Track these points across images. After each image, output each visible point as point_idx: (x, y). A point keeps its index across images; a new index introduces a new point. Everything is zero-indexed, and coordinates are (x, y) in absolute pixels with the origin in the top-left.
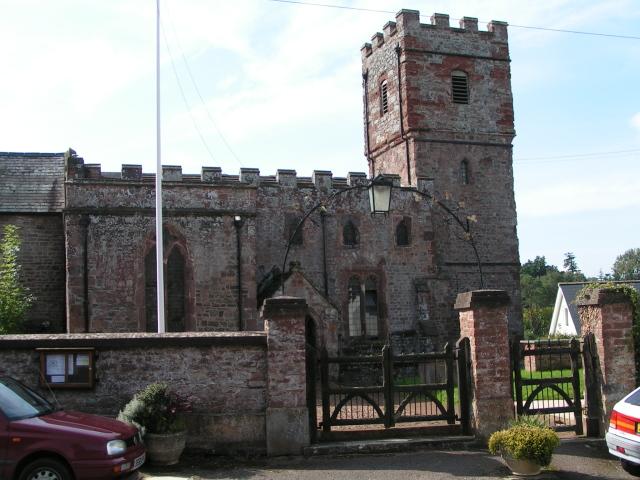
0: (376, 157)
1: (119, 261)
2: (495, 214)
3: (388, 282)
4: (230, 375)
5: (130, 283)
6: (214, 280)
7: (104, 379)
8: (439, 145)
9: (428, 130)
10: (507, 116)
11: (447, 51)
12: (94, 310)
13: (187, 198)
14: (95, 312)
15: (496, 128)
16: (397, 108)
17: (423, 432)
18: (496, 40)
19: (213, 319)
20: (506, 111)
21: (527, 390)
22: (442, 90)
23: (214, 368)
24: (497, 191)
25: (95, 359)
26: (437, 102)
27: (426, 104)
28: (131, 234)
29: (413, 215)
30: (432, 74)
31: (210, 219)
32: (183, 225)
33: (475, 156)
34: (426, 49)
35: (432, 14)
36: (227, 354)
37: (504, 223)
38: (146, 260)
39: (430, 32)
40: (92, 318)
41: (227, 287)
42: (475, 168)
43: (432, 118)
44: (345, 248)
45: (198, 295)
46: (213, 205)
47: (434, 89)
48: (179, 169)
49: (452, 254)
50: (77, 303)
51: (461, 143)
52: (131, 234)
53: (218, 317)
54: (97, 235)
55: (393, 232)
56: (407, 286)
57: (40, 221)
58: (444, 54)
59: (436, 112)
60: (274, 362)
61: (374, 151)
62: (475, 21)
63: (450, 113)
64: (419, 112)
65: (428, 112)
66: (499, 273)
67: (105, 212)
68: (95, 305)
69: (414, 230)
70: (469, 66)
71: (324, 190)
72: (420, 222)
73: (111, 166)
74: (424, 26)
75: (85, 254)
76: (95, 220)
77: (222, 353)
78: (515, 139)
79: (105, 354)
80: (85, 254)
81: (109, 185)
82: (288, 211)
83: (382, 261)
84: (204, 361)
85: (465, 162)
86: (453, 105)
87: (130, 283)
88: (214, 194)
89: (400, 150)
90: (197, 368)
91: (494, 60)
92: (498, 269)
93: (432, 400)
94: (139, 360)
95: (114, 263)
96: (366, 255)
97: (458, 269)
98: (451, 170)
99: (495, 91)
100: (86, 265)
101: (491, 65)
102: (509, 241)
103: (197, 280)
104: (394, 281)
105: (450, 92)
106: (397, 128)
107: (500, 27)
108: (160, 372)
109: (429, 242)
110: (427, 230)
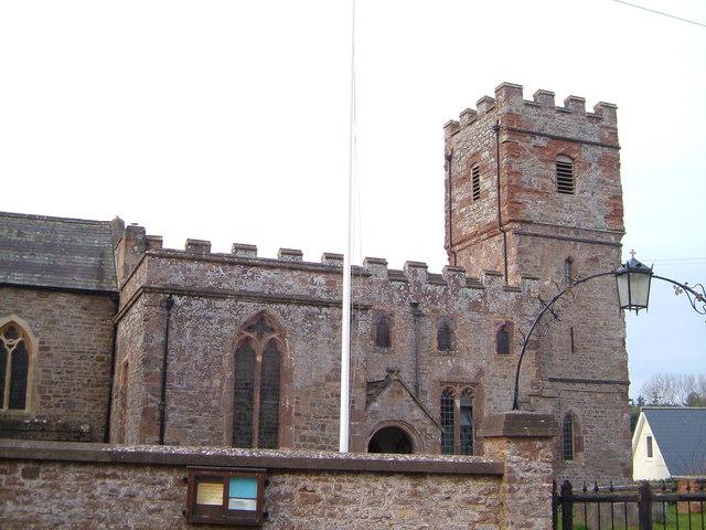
1: (206, 354)
2: (601, 324)
4: (450, 515)
5: (217, 382)
6: (317, 384)
7: (275, 512)
9: (530, 223)
11: (552, 133)
13: (290, 282)
14: (173, 418)
16: (493, 194)
19: (313, 433)
22: (547, 177)
23: (428, 504)
24: (604, 296)
25: (263, 485)
27: (528, 191)
28: (221, 322)
29: (516, 319)
31: (316, 309)
32: (283, 313)
33: (581, 255)
35: (535, 90)
36: (447, 486)
37: (611, 333)
38: (235, 356)
39: (533, 111)
40: (168, 424)
43: (534, 209)
44: (440, 355)
45: (297, 403)
46: (319, 293)
47: (537, 175)
48: (207, 245)
49: (553, 368)
50: (153, 405)
52: (221, 322)
53: (319, 430)
54: (181, 320)
57: (86, 301)
60: (513, 498)
61: (459, 243)
63: (555, 204)
67: (192, 293)
68: (172, 409)
69: (517, 338)
71: (418, 285)
72: (522, 328)
73: (175, 242)
74: (528, 104)
75: (166, 343)
76: (178, 301)
79: (279, 478)
80: (166, 343)
81: (199, 260)
83: (481, 373)
84: (415, 494)
85: (569, 261)
86: (557, 195)
88: (320, 279)
89: (495, 245)
90: (406, 503)
91: (603, 146)
92: (605, 387)
95: (199, 357)
96: (463, 364)
100: (166, 359)
101: (599, 151)
102: (617, 355)
103: (297, 384)
104: (492, 396)
105: (555, 179)
106: (493, 217)
107: (607, 112)
108: (354, 507)
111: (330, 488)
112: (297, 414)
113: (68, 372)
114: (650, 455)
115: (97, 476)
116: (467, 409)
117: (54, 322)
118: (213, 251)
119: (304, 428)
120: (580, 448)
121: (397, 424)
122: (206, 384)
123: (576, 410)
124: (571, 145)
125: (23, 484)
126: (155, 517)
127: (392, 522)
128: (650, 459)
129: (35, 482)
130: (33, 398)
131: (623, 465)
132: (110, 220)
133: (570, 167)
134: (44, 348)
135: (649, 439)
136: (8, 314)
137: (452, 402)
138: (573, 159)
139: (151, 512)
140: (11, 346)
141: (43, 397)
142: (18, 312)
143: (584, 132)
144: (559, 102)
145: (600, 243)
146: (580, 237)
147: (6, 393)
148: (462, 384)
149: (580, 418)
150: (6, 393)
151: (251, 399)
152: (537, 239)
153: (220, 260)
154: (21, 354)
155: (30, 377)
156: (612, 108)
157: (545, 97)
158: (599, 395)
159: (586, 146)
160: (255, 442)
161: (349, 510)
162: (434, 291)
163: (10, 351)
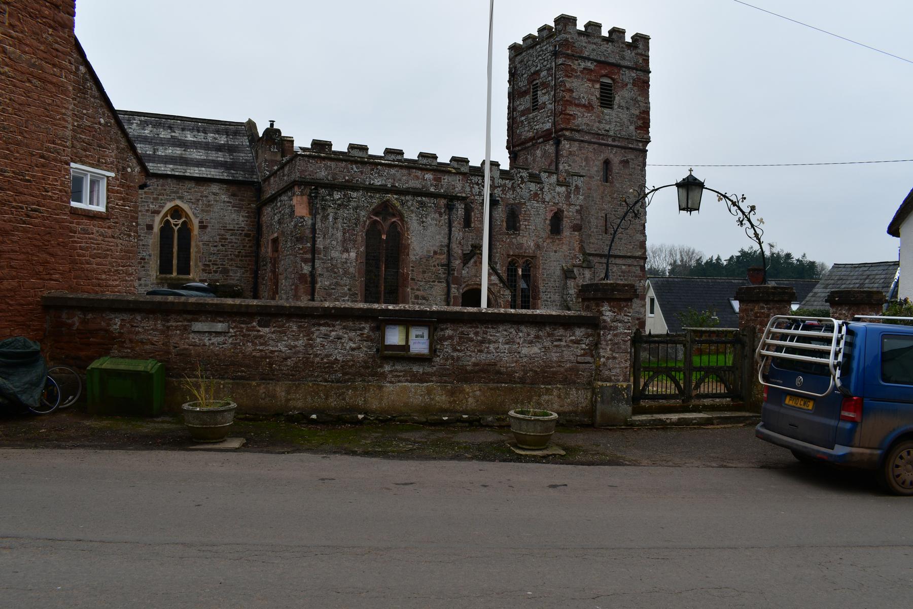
0: (519, 151)
8: (586, 145)
9: (578, 131)
12: (319, 279)
15: (634, 133)
17: (712, 408)
18: (640, 51)
21: (695, 376)
27: (578, 105)
32: (403, 204)
33: (616, 159)
41: (438, 265)
42: (616, 167)
44: (508, 234)
45: (413, 271)
48: (330, 145)
55: (548, 222)
56: (558, 272)
58: (595, 61)
59: (586, 114)
61: (518, 145)
65: (579, 114)
66: (629, 266)
67: (332, 187)
68: (321, 275)
69: (566, 223)
74: (580, 33)
75: (314, 225)
77: (555, 330)
80: (314, 225)
83: (538, 246)
84: (537, 337)
85: (607, 163)
87: (353, 255)
88: (429, 176)
90: (531, 342)
91: (637, 70)
92: (629, 261)
93: (723, 383)
94: (476, 334)
96: (524, 241)
98: (595, 169)
103: (412, 258)
105: (598, 96)
107: (641, 41)
111: (246, 330)
112: (413, 279)
113: (222, 245)
115: (314, 325)
116: (526, 276)
117: (209, 206)
118: (333, 149)
119: (418, 290)
122: (345, 255)
125: (259, 331)
126: (355, 353)
127: (522, 355)
129: (267, 330)
130: (196, 265)
131: (638, 319)
132: (245, 122)
133: (611, 87)
134: (203, 227)
135: (652, 300)
136: (174, 199)
137: (516, 271)
138: (613, 79)
139: (353, 349)
140: (176, 225)
141: (205, 265)
142: (181, 198)
146: (616, 143)
147: (175, 262)
148: (523, 257)
150: (175, 262)
151: (378, 267)
153: (339, 157)
154: (185, 230)
155: (193, 250)
157: (594, 27)
158: (624, 267)
159: (624, 69)
160: (382, 300)
161: (492, 347)
163: (176, 229)
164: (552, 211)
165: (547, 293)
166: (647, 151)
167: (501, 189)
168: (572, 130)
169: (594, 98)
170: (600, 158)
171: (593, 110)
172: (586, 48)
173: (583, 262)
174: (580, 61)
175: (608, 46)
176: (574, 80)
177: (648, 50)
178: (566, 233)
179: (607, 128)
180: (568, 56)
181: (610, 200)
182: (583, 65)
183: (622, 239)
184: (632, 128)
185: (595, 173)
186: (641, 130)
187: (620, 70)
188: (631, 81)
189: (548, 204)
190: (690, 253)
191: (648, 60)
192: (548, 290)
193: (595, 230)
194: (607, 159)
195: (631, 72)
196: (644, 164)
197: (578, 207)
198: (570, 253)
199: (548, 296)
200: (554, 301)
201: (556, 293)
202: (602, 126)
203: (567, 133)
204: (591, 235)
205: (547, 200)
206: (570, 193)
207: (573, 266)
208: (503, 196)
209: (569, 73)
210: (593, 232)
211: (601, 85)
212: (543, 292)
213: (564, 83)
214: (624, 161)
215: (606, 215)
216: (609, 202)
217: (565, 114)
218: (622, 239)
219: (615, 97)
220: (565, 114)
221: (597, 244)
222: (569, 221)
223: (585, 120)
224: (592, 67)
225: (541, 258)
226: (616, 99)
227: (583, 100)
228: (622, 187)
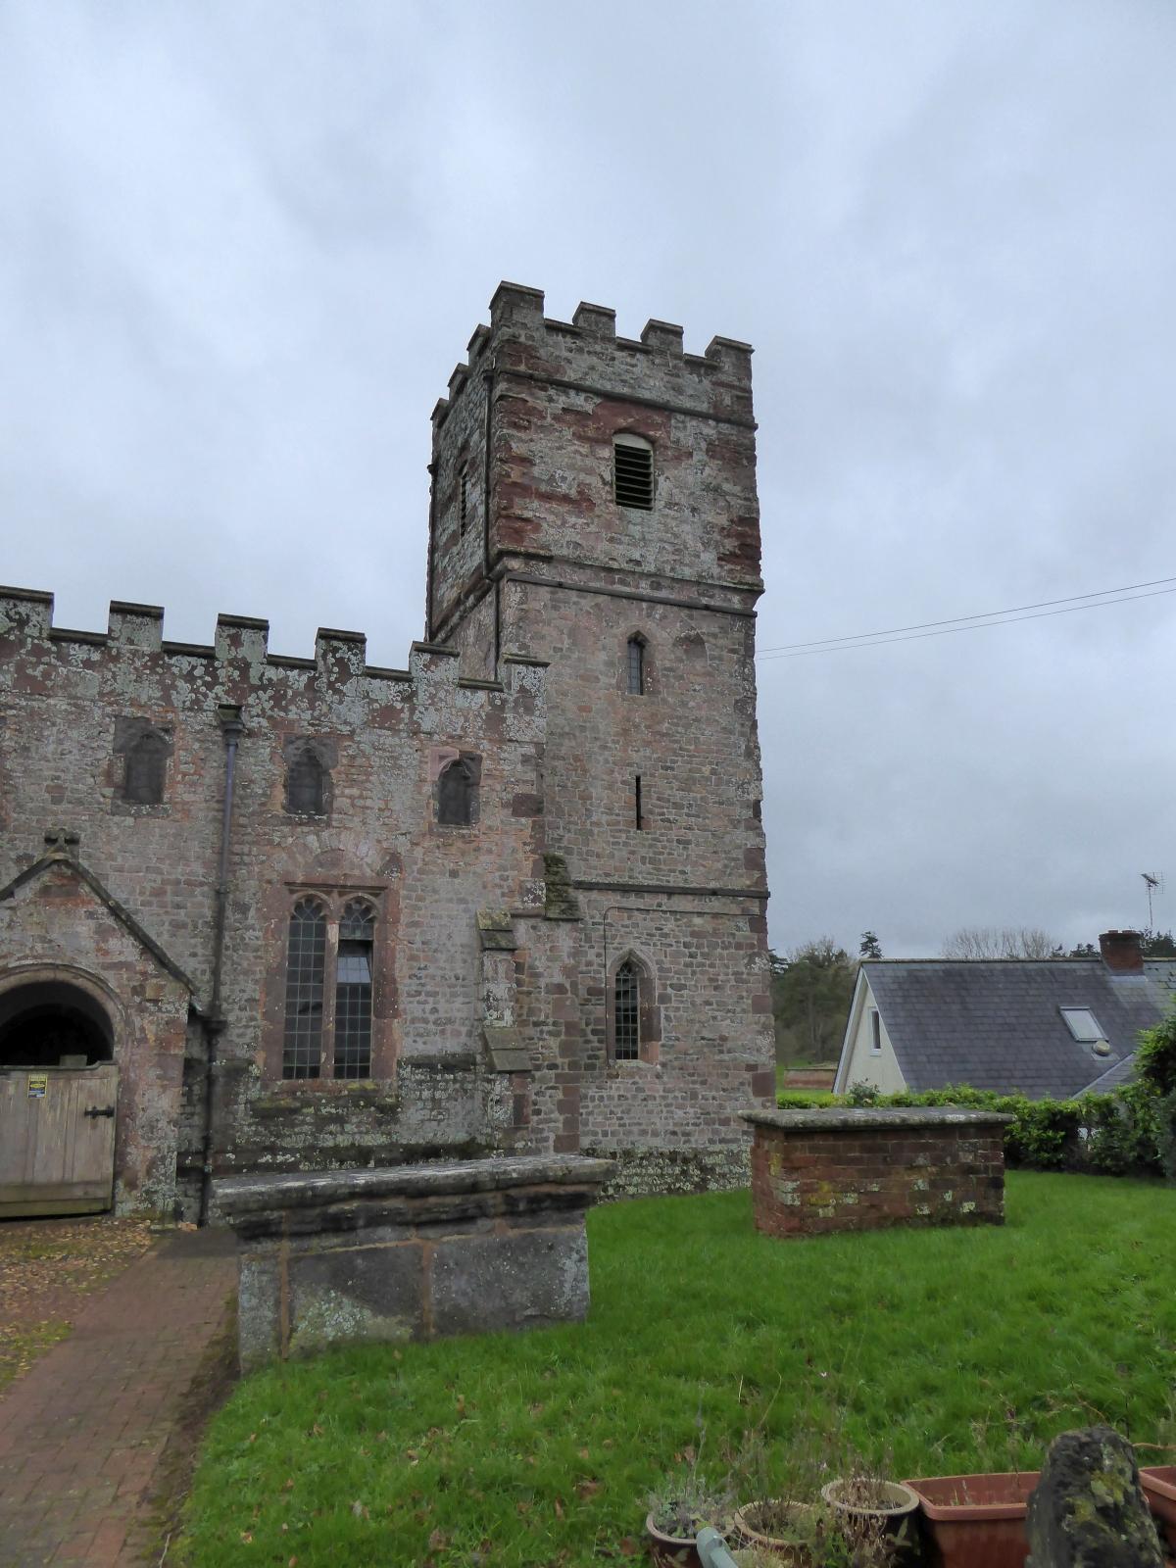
2: (706, 770)
3: (404, 919)
8: (573, 596)
9: (548, 560)
10: (742, 546)
15: (716, 571)
18: (723, 378)
20: (740, 536)
22: (590, 471)
26: (573, 493)
30: (568, 434)
33: (664, 632)
34: (558, 377)
44: (288, 822)
49: (593, 861)
51: (630, 597)
55: (428, 789)
56: (463, 935)
58: (598, 393)
59: (573, 520)
62: (677, 332)
64: (528, 514)
66: (716, 915)
69: (491, 794)
70: (658, 427)
74: (554, 327)
78: (761, 599)
80: (148, 947)
82: (127, 711)
83: (394, 860)
91: (718, 420)
92: (715, 904)
96: (346, 842)
97: (613, 899)
98: (603, 656)
99: (717, 489)
101: (710, 429)
105: (608, 477)
107: (731, 355)
109: (526, 821)
110: (519, 789)
114: (878, 1046)
120: (651, 1034)
121: (62, 976)
123: (645, 953)
124: (649, 413)
128: (877, 1051)
135: (876, 1016)
138: (652, 441)
143: (678, 390)
144: (629, 328)
145: (707, 608)
146: (663, 594)
148: (343, 890)
149: (654, 968)
152: (561, 594)
156: (741, 353)
157: (595, 319)
158: (697, 921)
159: (681, 417)
162: (284, 682)
164: (442, 758)
165: (422, 998)
166: (755, 615)
167: (270, 692)
168: (529, 557)
169: (595, 481)
170: (615, 631)
171: (592, 510)
172: (569, 362)
173: (549, 902)
174: (552, 392)
175: (634, 361)
176: (535, 437)
177: (749, 377)
178: (492, 813)
179: (637, 556)
180: (517, 378)
181: (649, 737)
182: (562, 401)
183: (688, 842)
184: (709, 558)
185: (602, 668)
186: (734, 563)
187: (669, 418)
188: (704, 445)
189: (431, 740)
190: (1039, 942)
191: (750, 399)
192: (428, 988)
193: (604, 818)
194: (638, 633)
195: (701, 425)
196: (749, 650)
197: (531, 750)
198: (504, 879)
199: (428, 1007)
200: (450, 1021)
201: (454, 995)
202: (619, 550)
203: (515, 564)
204: (591, 833)
205: (426, 726)
206: (502, 708)
207: (513, 916)
208: (279, 714)
209: (523, 418)
210: (598, 824)
211: (617, 452)
212: (409, 995)
213: (507, 442)
214: (687, 638)
215: (638, 779)
216: (648, 744)
217: (508, 517)
218: (688, 842)
219: (656, 483)
220: (508, 517)
221: (612, 856)
222: (498, 787)
223: (571, 535)
224: (589, 408)
225: (403, 892)
226: (660, 486)
227: (564, 486)
228: (684, 704)
